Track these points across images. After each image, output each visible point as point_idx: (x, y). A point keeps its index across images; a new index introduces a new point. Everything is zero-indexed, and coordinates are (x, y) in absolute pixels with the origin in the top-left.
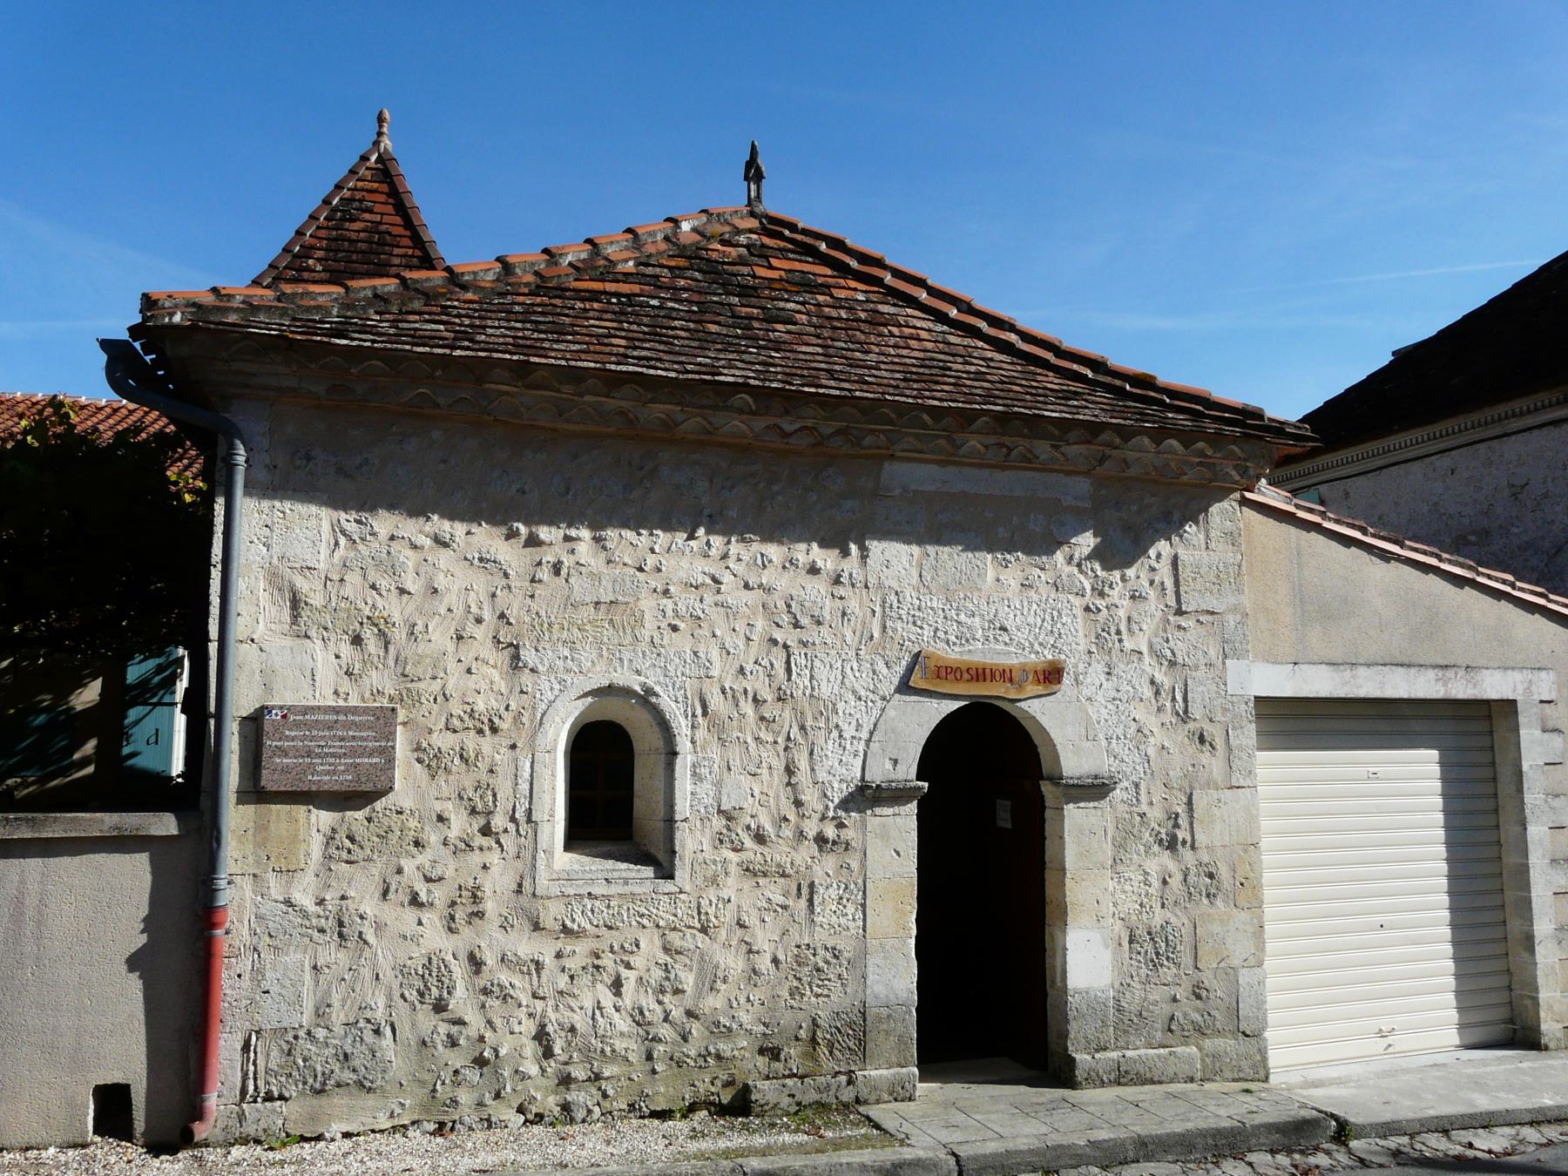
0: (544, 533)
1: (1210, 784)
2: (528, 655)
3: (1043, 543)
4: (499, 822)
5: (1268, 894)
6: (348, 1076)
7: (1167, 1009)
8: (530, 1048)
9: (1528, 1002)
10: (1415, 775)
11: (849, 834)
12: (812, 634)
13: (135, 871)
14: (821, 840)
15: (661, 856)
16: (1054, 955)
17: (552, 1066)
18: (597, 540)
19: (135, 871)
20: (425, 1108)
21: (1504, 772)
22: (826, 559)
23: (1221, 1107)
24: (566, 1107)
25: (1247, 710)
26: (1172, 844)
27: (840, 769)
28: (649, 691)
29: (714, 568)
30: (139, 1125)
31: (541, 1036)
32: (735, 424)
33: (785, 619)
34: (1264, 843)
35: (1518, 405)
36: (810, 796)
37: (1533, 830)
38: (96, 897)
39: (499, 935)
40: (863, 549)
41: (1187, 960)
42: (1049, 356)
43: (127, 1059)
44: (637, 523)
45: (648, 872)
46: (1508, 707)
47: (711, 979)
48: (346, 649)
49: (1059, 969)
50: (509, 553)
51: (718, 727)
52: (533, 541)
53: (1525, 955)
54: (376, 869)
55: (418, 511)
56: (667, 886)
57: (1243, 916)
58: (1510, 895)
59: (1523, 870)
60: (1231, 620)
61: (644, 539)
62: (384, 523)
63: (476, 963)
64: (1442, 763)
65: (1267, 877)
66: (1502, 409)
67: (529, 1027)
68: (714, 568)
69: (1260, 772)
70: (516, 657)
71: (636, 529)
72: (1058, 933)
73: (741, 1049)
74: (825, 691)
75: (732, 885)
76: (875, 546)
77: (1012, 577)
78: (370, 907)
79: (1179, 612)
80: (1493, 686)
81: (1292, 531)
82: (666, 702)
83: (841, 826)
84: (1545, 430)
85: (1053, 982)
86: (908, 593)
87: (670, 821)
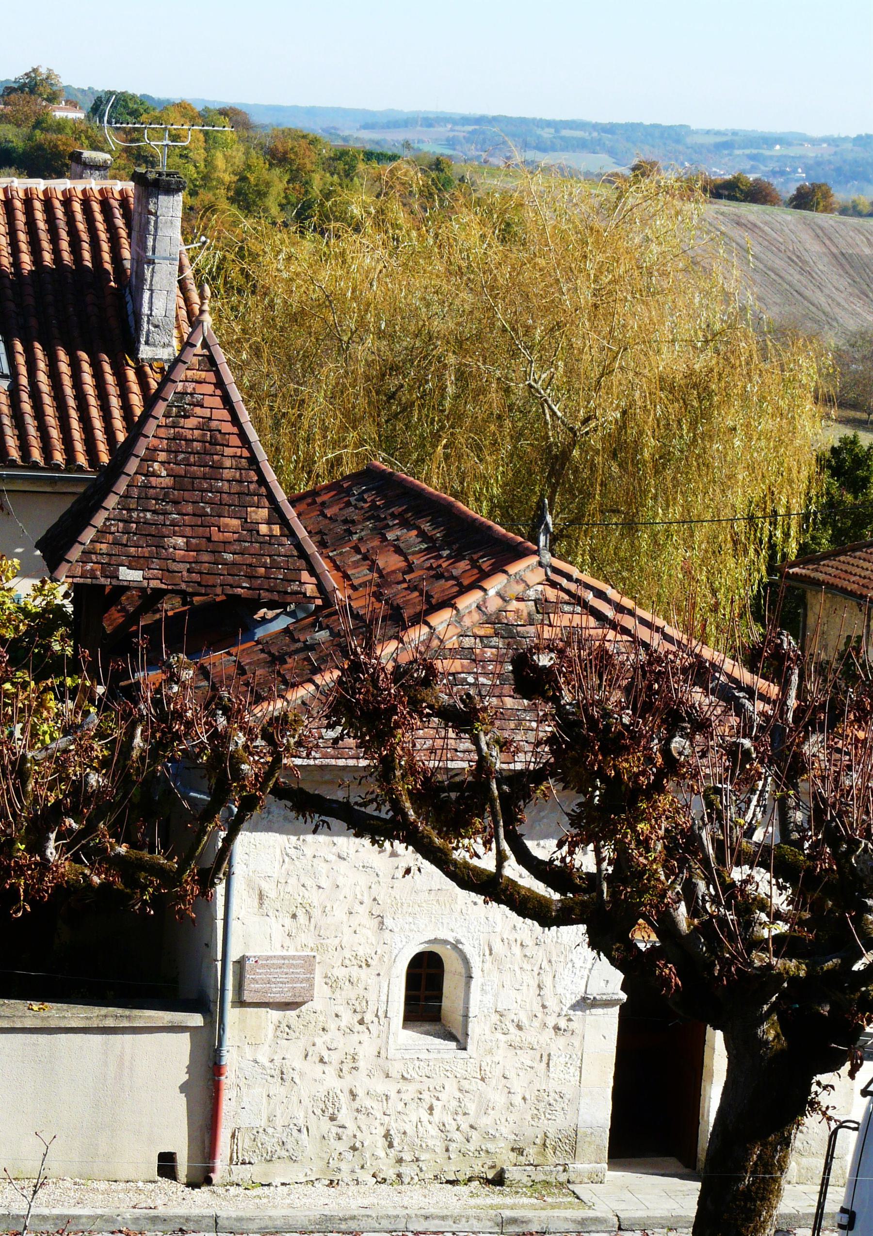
2: (388, 922)
4: (369, 1017)
11: (573, 1025)
14: (557, 1028)
15: (459, 1037)
17: (392, 1153)
31: (387, 1135)
36: (552, 1003)
38: (154, 1053)
43: (179, 1143)
45: (453, 1045)
48: (288, 921)
54: (302, 1043)
63: (353, 1095)
78: (298, 1063)
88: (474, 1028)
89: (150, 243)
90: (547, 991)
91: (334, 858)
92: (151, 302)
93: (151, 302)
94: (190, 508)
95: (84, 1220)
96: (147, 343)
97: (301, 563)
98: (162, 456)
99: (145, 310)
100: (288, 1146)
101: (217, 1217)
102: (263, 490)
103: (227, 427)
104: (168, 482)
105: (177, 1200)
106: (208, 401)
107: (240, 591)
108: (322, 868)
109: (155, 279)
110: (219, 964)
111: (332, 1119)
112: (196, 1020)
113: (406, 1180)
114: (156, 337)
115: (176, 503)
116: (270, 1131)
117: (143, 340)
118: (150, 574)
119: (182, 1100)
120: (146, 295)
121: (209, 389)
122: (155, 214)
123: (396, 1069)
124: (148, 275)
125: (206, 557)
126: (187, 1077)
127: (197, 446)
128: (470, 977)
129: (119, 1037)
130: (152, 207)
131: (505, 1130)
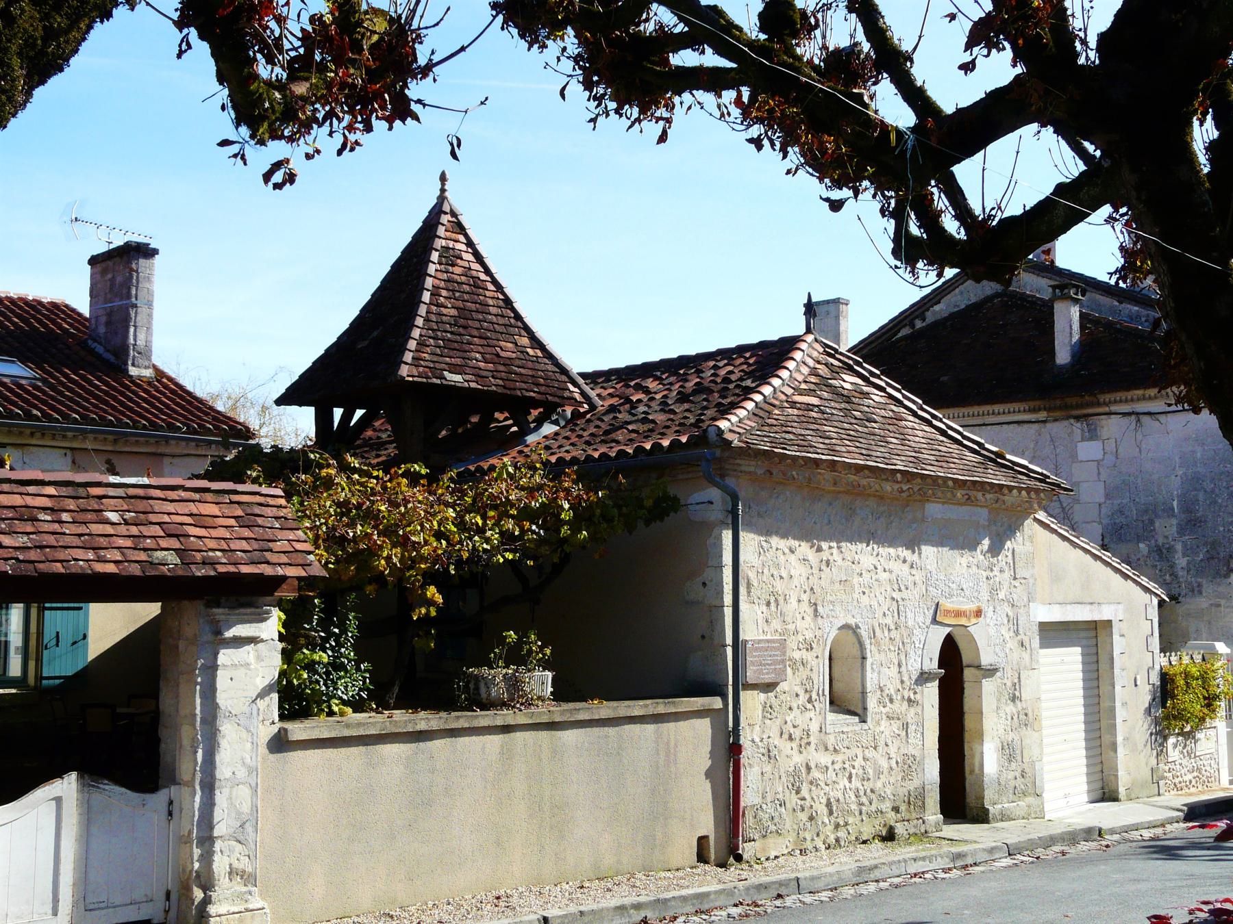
0: (825, 545)
1: (1025, 668)
2: (820, 608)
3: (972, 546)
4: (814, 696)
5: (1044, 723)
6: (773, 828)
7: (1012, 783)
8: (825, 811)
9: (1112, 778)
10: (1071, 658)
11: (918, 697)
12: (905, 594)
13: (704, 727)
14: (909, 700)
15: (859, 711)
16: (973, 756)
17: (833, 819)
18: (839, 548)
19: (704, 727)
20: (795, 843)
21: (1103, 657)
22: (904, 552)
23: (1038, 830)
24: (837, 840)
25: (1036, 628)
26: (1014, 699)
27: (914, 666)
28: (857, 627)
29: (875, 562)
30: (713, 857)
31: (829, 804)
32: (888, 487)
33: (896, 587)
34: (1043, 697)
35: (997, 408)
36: (905, 678)
37: (1118, 688)
38: (692, 739)
39: (814, 753)
40: (920, 549)
41: (1019, 758)
42: (959, 437)
43: (706, 824)
44: (851, 540)
45: (857, 719)
46: (1108, 623)
47: (879, 773)
48: (764, 608)
49: (977, 764)
50: (811, 554)
51: (878, 644)
52: (819, 550)
53: (1112, 754)
54: (778, 722)
55: (784, 536)
56: (865, 726)
57: (1036, 735)
58: (1104, 723)
59: (1112, 710)
60: (1031, 581)
61: (853, 547)
62: (775, 541)
63: (808, 768)
64: (1083, 655)
65: (1044, 714)
66: (989, 408)
67: (824, 801)
68: (875, 562)
69: (1041, 660)
70: (816, 610)
71: (851, 542)
72: (976, 747)
73: (886, 806)
74: (910, 623)
75: (884, 723)
76: (923, 547)
77: (964, 561)
78: (776, 741)
79: (1015, 579)
80: (1104, 614)
81: (1047, 533)
82: (864, 633)
83: (915, 693)
84: (1012, 426)
85: (972, 771)
86: (934, 572)
87: (864, 693)
88: (872, 703)
89: (134, 292)
90: (903, 669)
91: (787, 551)
92: (135, 336)
93: (135, 336)
94: (475, 333)
95: (712, 896)
96: (133, 365)
97: (564, 378)
98: (444, 293)
99: (132, 341)
100: (776, 820)
101: (798, 879)
102: (520, 324)
103: (483, 277)
104: (453, 312)
105: (710, 880)
106: (465, 256)
107: (532, 394)
108: (782, 559)
109: (139, 318)
110: (729, 651)
111: (798, 792)
112: (717, 703)
113: (842, 843)
114: (140, 361)
115: (465, 327)
116: (764, 806)
117: (130, 363)
118: (468, 377)
119: (707, 785)
120: (132, 330)
121: (463, 247)
122: (137, 271)
123: (831, 740)
124: (133, 315)
125: (501, 368)
126: (709, 763)
127: (467, 288)
128: (864, 658)
129: (671, 725)
130: (134, 266)
131: (889, 791)
